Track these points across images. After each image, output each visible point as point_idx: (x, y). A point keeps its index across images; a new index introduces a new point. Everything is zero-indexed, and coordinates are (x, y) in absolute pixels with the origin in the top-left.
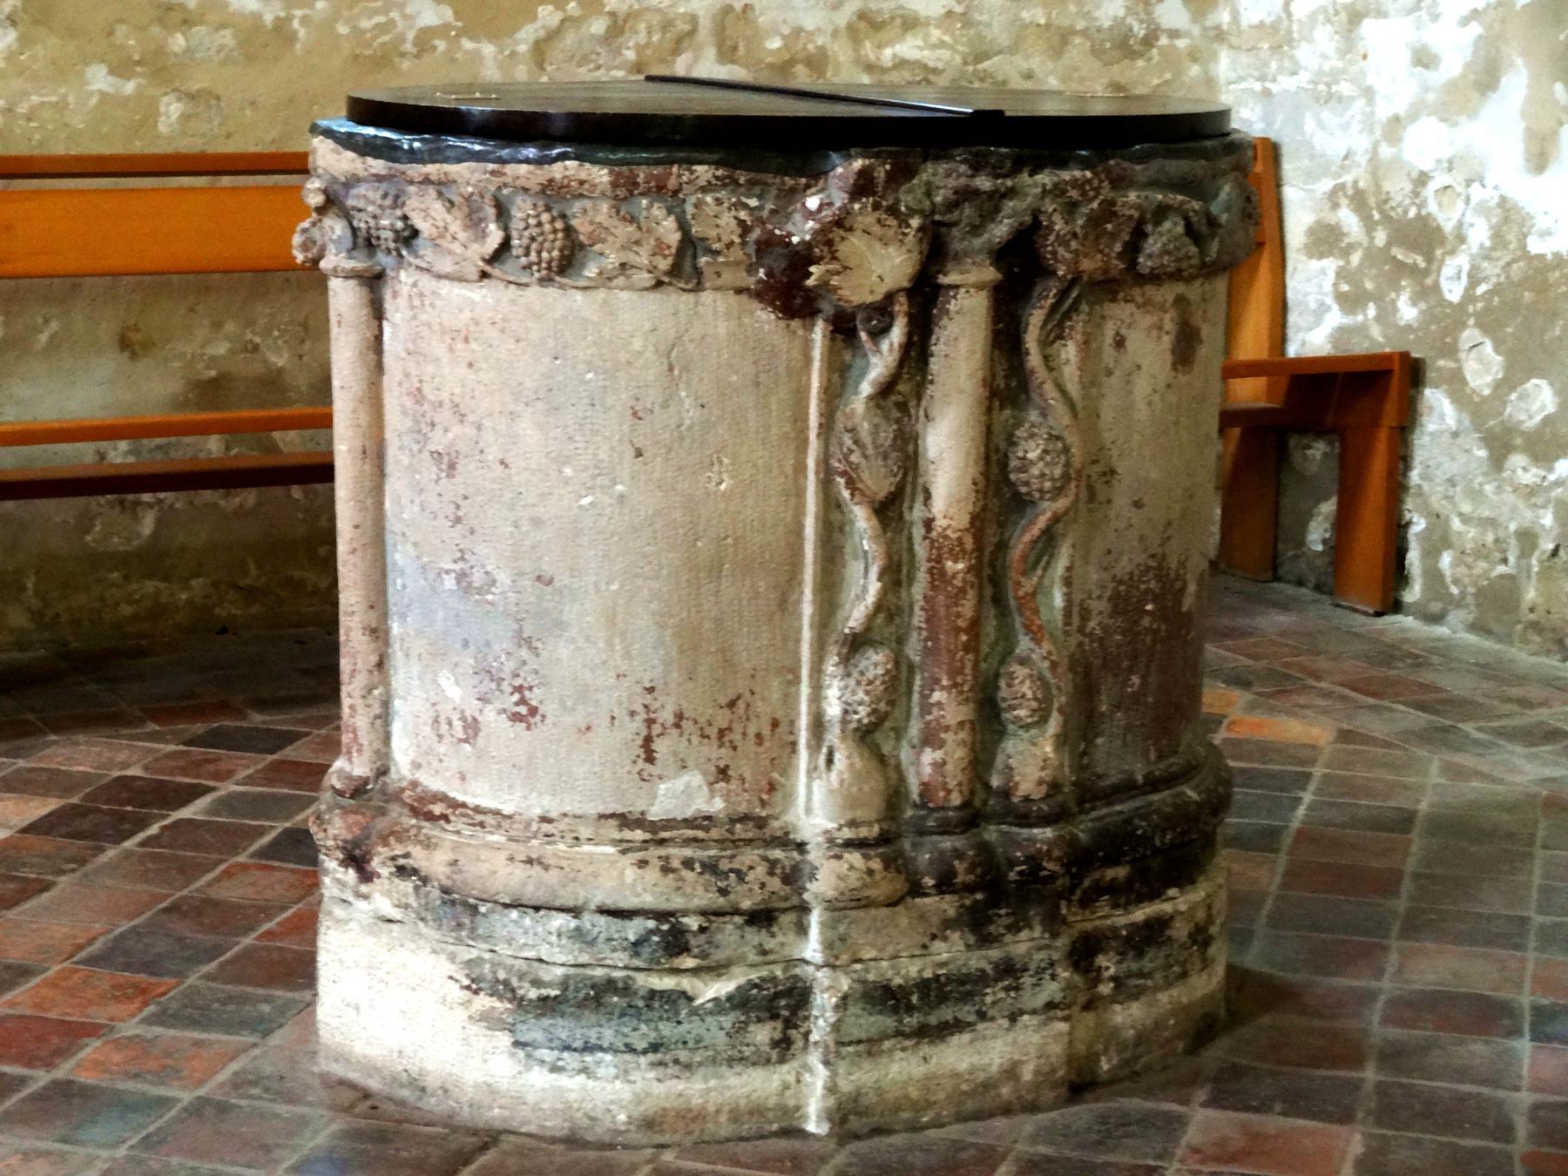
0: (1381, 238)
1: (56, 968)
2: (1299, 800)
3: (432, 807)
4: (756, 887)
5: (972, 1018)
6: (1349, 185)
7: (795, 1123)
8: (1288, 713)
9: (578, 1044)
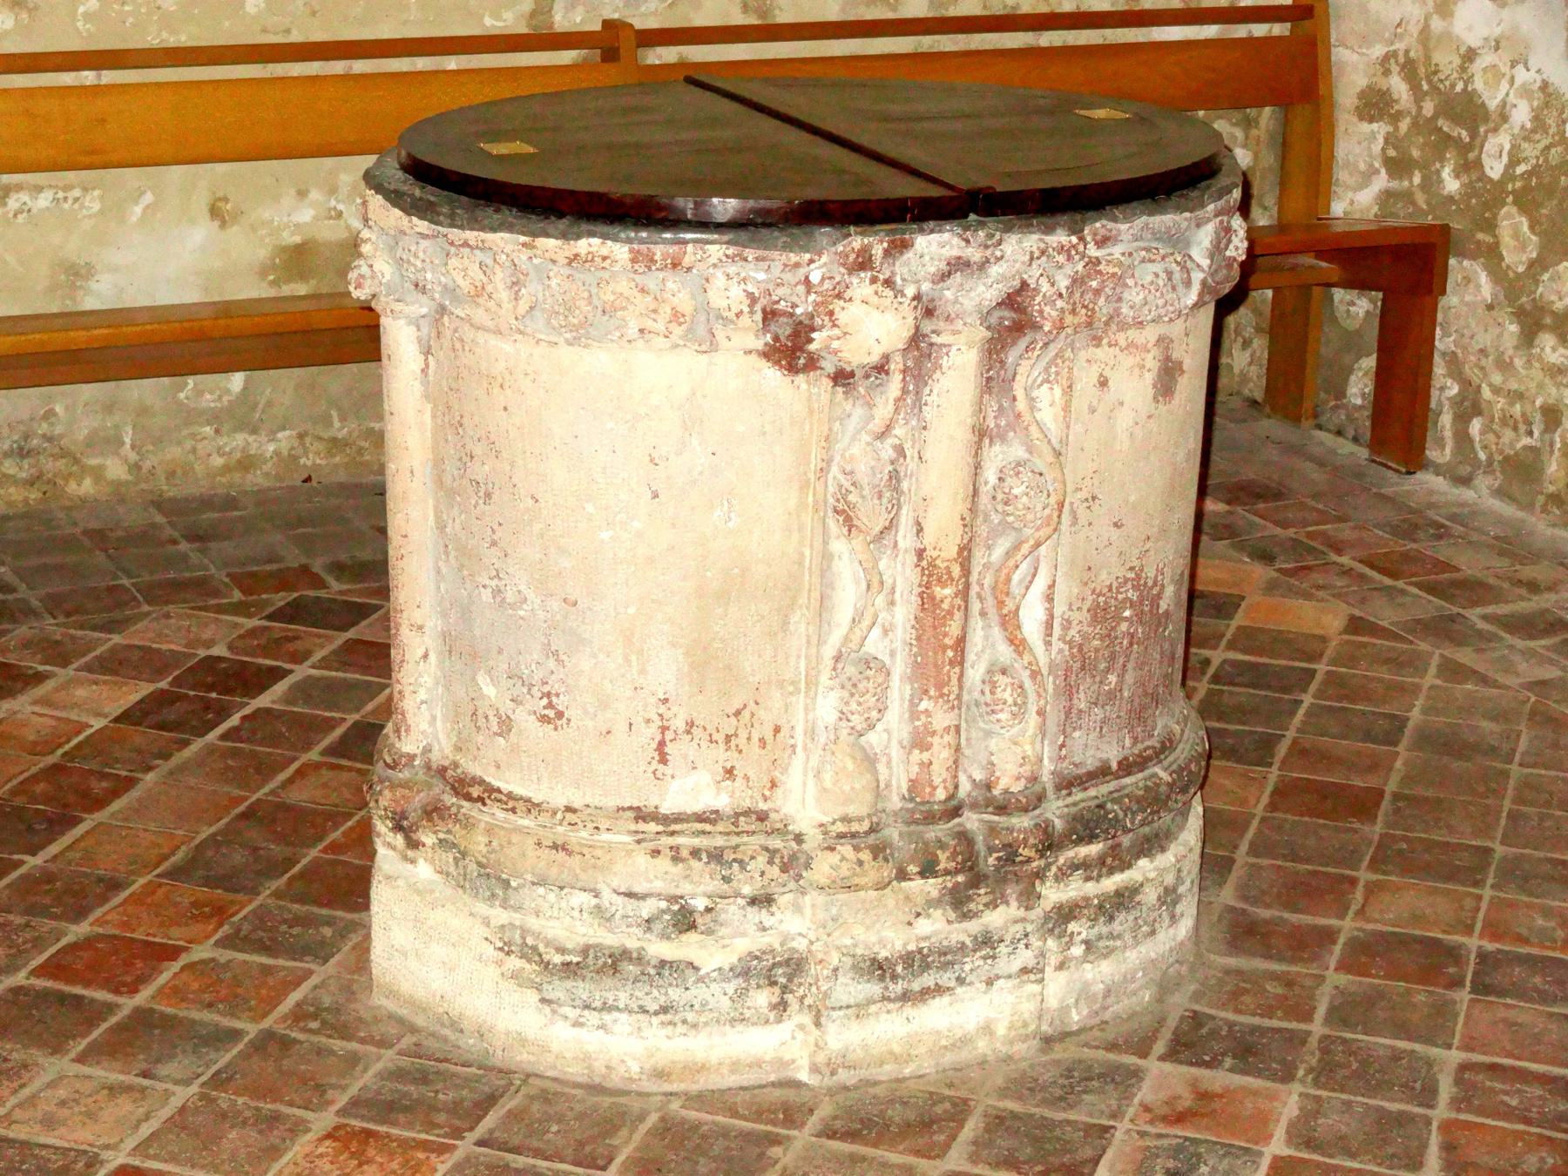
0: (1429, 108)
1: (142, 881)
2: (1299, 703)
3: (471, 790)
4: (757, 875)
5: (952, 984)
6: (1401, 54)
7: (790, 1074)
8: (1308, 596)
9: (597, 1004)
